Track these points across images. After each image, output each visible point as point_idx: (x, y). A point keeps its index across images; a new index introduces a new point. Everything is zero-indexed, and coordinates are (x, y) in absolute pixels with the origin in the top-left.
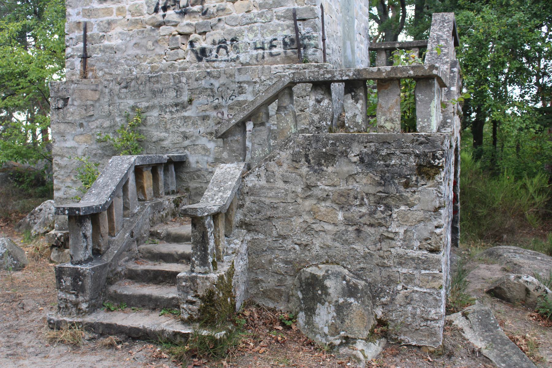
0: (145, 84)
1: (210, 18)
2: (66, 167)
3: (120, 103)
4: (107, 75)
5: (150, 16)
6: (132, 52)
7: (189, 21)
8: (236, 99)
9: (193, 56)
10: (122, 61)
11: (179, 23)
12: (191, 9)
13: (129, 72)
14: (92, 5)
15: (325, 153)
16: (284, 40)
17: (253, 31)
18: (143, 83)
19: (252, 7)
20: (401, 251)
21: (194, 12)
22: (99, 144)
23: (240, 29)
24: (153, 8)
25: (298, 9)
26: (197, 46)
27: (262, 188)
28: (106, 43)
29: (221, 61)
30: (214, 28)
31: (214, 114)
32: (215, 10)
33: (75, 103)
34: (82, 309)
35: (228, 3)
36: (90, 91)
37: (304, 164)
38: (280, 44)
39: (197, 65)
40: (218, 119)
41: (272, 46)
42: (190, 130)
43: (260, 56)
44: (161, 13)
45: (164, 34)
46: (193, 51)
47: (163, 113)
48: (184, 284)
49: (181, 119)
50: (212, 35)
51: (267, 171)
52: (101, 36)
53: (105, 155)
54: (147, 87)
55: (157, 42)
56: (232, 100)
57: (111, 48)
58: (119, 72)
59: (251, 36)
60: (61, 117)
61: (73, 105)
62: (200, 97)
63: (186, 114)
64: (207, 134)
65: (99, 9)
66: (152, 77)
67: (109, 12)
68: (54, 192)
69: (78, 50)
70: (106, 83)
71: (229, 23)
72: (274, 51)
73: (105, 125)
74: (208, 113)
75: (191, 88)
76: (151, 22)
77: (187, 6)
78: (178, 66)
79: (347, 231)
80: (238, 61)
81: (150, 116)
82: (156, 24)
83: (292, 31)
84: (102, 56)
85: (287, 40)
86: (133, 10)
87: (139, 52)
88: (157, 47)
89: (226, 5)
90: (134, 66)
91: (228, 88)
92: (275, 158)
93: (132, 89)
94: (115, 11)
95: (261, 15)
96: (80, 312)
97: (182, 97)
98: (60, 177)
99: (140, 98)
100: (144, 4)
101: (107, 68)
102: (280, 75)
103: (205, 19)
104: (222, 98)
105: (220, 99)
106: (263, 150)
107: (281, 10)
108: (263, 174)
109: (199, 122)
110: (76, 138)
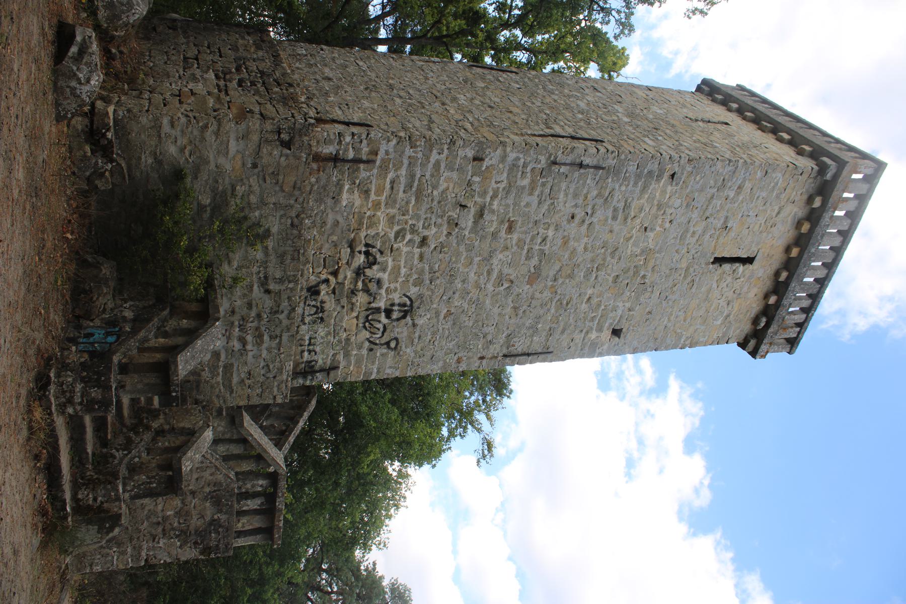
0: (292, 246)
2: (203, 139)
4: (309, 187)
7: (349, 277)
15: (221, 501)
17: (327, 335)
20: (145, 546)
21: (357, 282)
22: (229, 187)
24: (370, 242)
28: (347, 187)
29: (304, 309)
31: (253, 314)
33: (283, 159)
34: (66, 408)
36: (294, 179)
41: (310, 351)
43: (303, 343)
44: (364, 249)
46: (319, 283)
48: (113, 494)
49: (250, 282)
53: (216, 194)
55: (336, 246)
57: (340, 193)
58: (311, 204)
59: (322, 334)
63: (255, 287)
65: (385, 181)
67: (379, 192)
69: (346, 150)
70: (301, 200)
72: (306, 354)
74: (254, 308)
76: (357, 239)
77: (364, 276)
79: (158, 517)
83: (320, 366)
85: (313, 363)
86: (375, 219)
87: (329, 226)
93: (289, 231)
94: (379, 198)
95: (340, 341)
98: (190, 129)
105: (267, 320)
107: (340, 357)
110: (240, 156)
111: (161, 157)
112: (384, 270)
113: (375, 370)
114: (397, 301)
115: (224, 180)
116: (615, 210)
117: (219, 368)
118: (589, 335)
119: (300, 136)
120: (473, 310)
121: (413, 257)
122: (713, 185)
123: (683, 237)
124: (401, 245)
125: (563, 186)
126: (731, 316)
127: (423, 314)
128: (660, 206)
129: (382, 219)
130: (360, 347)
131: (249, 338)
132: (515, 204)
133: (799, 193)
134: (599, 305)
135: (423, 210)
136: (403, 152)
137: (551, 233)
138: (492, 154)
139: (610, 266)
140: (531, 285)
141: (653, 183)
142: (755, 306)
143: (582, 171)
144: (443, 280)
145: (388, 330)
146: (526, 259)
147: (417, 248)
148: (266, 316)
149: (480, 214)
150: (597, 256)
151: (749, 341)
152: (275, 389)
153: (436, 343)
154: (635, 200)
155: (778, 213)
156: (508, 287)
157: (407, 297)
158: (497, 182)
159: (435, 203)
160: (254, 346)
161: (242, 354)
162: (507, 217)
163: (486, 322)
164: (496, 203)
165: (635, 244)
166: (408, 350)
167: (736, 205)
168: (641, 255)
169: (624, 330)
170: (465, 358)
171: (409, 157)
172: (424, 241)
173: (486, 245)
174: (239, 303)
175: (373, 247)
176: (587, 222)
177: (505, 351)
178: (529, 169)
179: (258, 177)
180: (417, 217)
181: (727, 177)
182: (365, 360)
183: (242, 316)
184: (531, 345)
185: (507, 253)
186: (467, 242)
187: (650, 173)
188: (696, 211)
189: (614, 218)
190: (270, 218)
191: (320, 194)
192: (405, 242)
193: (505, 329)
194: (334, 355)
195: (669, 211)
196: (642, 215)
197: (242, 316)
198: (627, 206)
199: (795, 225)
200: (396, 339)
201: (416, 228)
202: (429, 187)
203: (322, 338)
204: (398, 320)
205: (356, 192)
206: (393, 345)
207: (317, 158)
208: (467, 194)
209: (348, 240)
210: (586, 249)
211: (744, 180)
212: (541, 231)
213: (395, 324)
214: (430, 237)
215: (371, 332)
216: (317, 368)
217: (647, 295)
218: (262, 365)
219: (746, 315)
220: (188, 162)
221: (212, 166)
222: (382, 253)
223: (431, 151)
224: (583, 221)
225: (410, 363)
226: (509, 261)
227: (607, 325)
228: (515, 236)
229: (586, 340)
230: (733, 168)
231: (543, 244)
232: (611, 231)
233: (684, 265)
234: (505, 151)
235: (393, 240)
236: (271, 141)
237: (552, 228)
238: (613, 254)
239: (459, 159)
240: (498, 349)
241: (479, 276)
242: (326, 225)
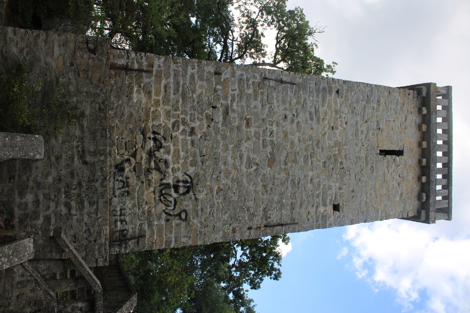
0: (101, 126)
1: (145, 174)
2: (36, 44)
3: (87, 102)
4: (111, 87)
5: (150, 127)
6: (127, 111)
7: (144, 158)
8: (86, 200)
11: (144, 150)
12: (152, 160)
13: (111, 107)
14: (164, 79)
16: (125, 230)
18: (102, 124)
19: (149, 205)
23: (135, 198)
24: (156, 130)
25: (145, 238)
26: (126, 165)
27: (13, 279)
28: (135, 89)
29: (114, 184)
30: (138, 178)
32: (150, 178)
33: (90, 61)
35: (154, 188)
36: (99, 75)
37: (33, 309)
38: (123, 227)
39: (112, 164)
40: (71, 186)
41: (122, 221)
42: (63, 163)
43: (115, 213)
44: (152, 136)
45: (137, 138)
46: (123, 161)
47: (77, 140)
49: (72, 155)
50: (133, 177)
51: (27, 281)
52: (141, 85)
54: (98, 127)
56: (85, 197)
57: (131, 93)
58: (112, 99)
59: (130, 206)
60: (80, 45)
61: (89, 58)
62: (88, 171)
63: (76, 159)
64: (60, 176)
65: (160, 85)
66: (106, 131)
67: (158, 93)
68: (13, 28)
69: (133, 63)
70: (105, 90)
71: (140, 189)
72: (119, 223)
73: (71, 87)
74: (76, 177)
75: (95, 163)
76: (147, 128)
77: (155, 157)
78: (113, 149)
80: (113, 196)
81: (76, 128)
82: (145, 132)
84: (126, 84)
85: (126, 231)
87: (126, 117)
88: (128, 132)
89: (152, 187)
90: (115, 112)
91: (94, 193)
92: (37, 287)
93: (98, 114)
94: (158, 98)
95: (143, 213)
97: (89, 156)
98: (27, 37)
100: (160, 123)
101: (116, 88)
102: (101, 232)
103: (145, 171)
104: (87, 189)
106: (44, 270)
107: (146, 227)
108: (24, 278)
109: (69, 170)
110: (61, 58)
111: (6, 55)
112: (168, 152)
113: (173, 239)
114: (181, 178)
115: (51, 73)
116: (310, 113)
117: (50, 232)
118: (319, 209)
119: (102, 46)
120: (236, 187)
121: (187, 143)
122: (363, 99)
123: (356, 135)
124: (177, 133)
125: (275, 94)
126: (404, 195)
127: (201, 190)
128: (336, 112)
129: (162, 113)
130: (159, 218)
131: (73, 204)
132: (247, 106)
133: (412, 106)
134: (319, 185)
135: (189, 107)
136: (169, 66)
137: (274, 128)
138: (226, 71)
139: (318, 154)
140: (271, 167)
141: (328, 95)
142: (416, 188)
143: (283, 85)
144: (211, 162)
145: (178, 203)
146: (263, 147)
147: (189, 136)
148: (85, 184)
149: (226, 113)
150: (308, 146)
151: (421, 212)
152: (97, 252)
153: (215, 215)
154: (321, 107)
155: (406, 120)
156: (256, 169)
157: (188, 175)
158: (233, 90)
159: (196, 103)
160: (77, 211)
161: (68, 219)
162: (244, 115)
163: (246, 197)
164: (235, 104)
165: (330, 139)
166: (195, 221)
167: (380, 113)
168: (335, 146)
169: (340, 205)
170: (238, 229)
171: (174, 70)
172: (192, 131)
173: (234, 136)
174: (64, 172)
175: (159, 134)
176: (296, 122)
177: (265, 222)
178: (250, 82)
179: (74, 72)
180: (185, 112)
181: (369, 94)
182: (165, 230)
183: (67, 184)
184: (281, 217)
185: (250, 142)
186: (222, 133)
187: (324, 88)
188: (358, 117)
189: (312, 119)
190: (84, 103)
191: (118, 92)
192: (180, 132)
193: (261, 203)
194: (141, 225)
195: (343, 116)
196: (328, 117)
197: (67, 184)
198: (317, 111)
199: (418, 129)
200: (185, 211)
201: (186, 121)
202: (190, 91)
203: (130, 209)
204: (184, 194)
205: (142, 92)
206: (183, 216)
207: (113, 67)
208: (215, 98)
209: (140, 128)
210: (299, 141)
211: (379, 97)
212: (269, 127)
213: (182, 197)
214: (196, 128)
215: (166, 205)
216: (128, 236)
217: (347, 177)
218: (85, 228)
219: (412, 193)
220: (26, 60)
221: (43, 64)
222: (165, 139)
223: (187, 66)
224: (293, 120)
225: (198, 233)
226: (253, 148)
227: (328, 200)
228: (252, 130)
229: (318, 213)
230: (370, 88)
231: (271, 136)
232: (312, 129)
233: (363, 155)
234: (233, 69)
235: (171, 129)
236: (82, 48)
237: (274, 125)
238: (317, 145)
239: (205, 73)
240: (260, 221)
241: (234, 159)
242: (124, 116)
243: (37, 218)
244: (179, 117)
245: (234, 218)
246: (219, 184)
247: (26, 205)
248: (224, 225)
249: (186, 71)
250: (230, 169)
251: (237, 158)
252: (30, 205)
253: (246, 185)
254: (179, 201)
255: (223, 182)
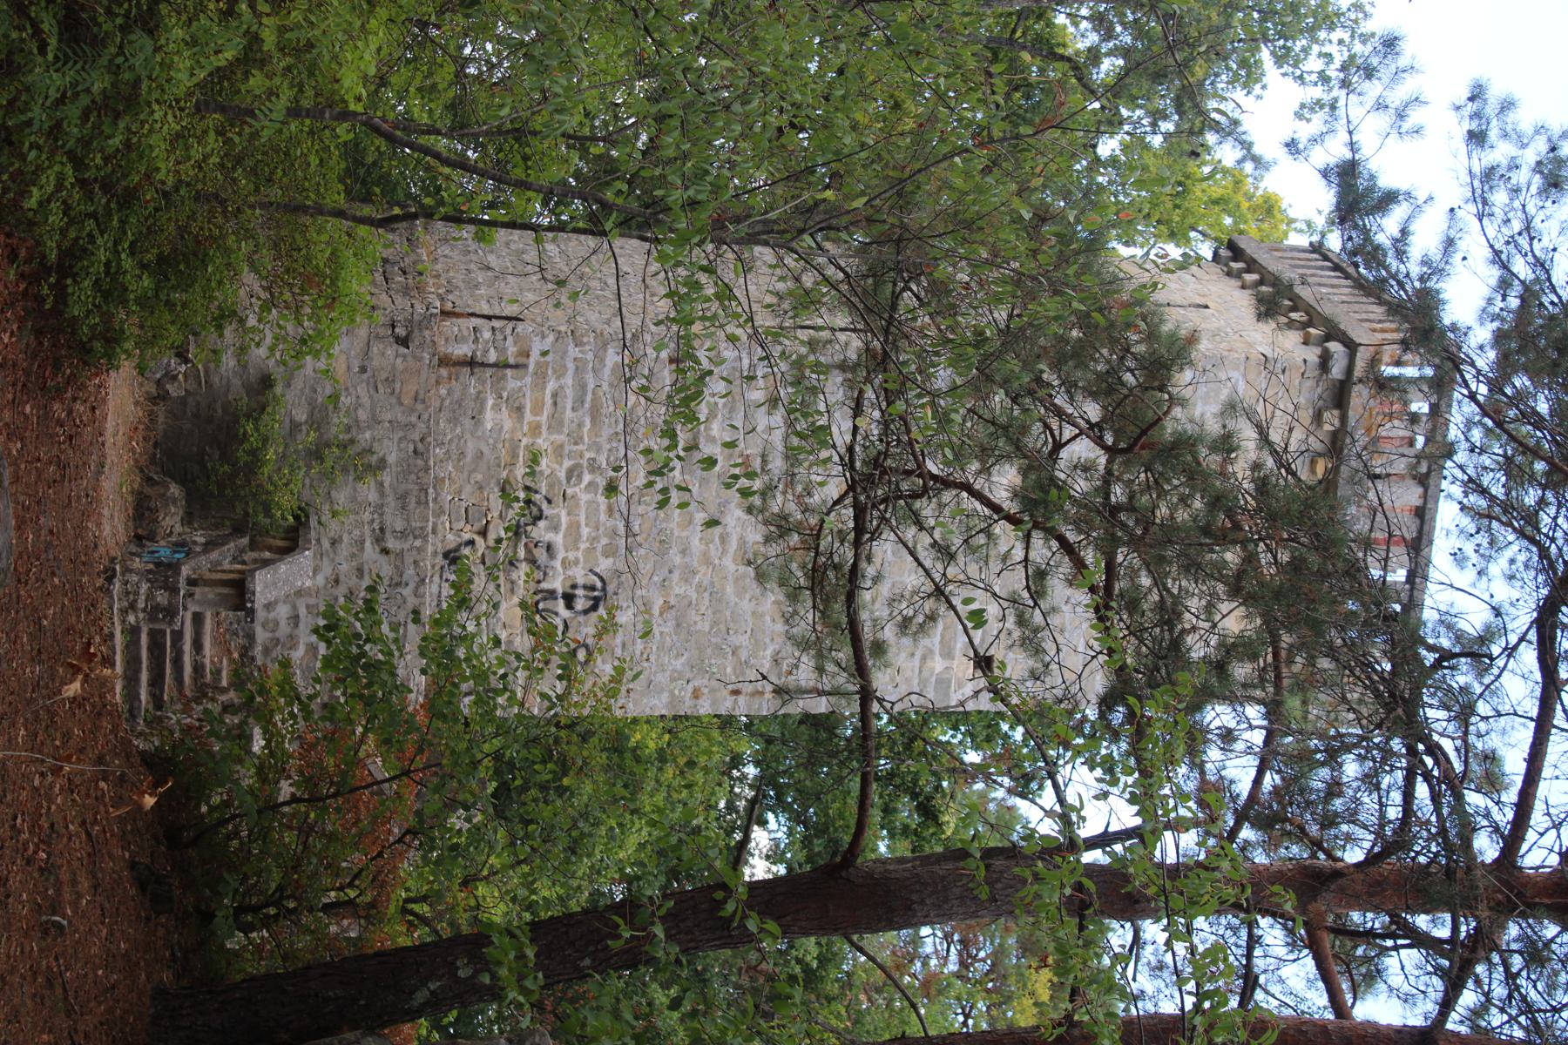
6: (471, 448)
9: (452, 546)
10: (458, 431)
21: (516, 547)
26: (466, 551)
28: (490, 402)
33: (399, 361)
42: (344, 549)
55: (481, 488)
57: (481, 410)
63: (368, 544)
67: (537, 409)
69: (486, 351)
70: (425, 417)
74: (366, 577)
87: (469, 458)
96: (124, 612)
99: (398, 473)
109: (354, 564)
112: (555, 528)
114: (580, 581)
118: (929, 664)
124: (577, 489)
136: (565, 352)
153: (652, 658)
157: (596, 574)
193: (767, 640)
204: (586, 612)
207: (445, 361)
213: (581, 618)
222: (549, 502)
229: (925, 674)
243: (294, 647)
244: (581, 456)
245: (699, 667)
246: (668, 595)
247: (277, 624)
248: (673, 680)
249: (602, 361)
250: (695, 564)
251: (712, 541)
252: (283, 623)
253: (733, 599)
254: (573, 625)
255: (677, 590)
